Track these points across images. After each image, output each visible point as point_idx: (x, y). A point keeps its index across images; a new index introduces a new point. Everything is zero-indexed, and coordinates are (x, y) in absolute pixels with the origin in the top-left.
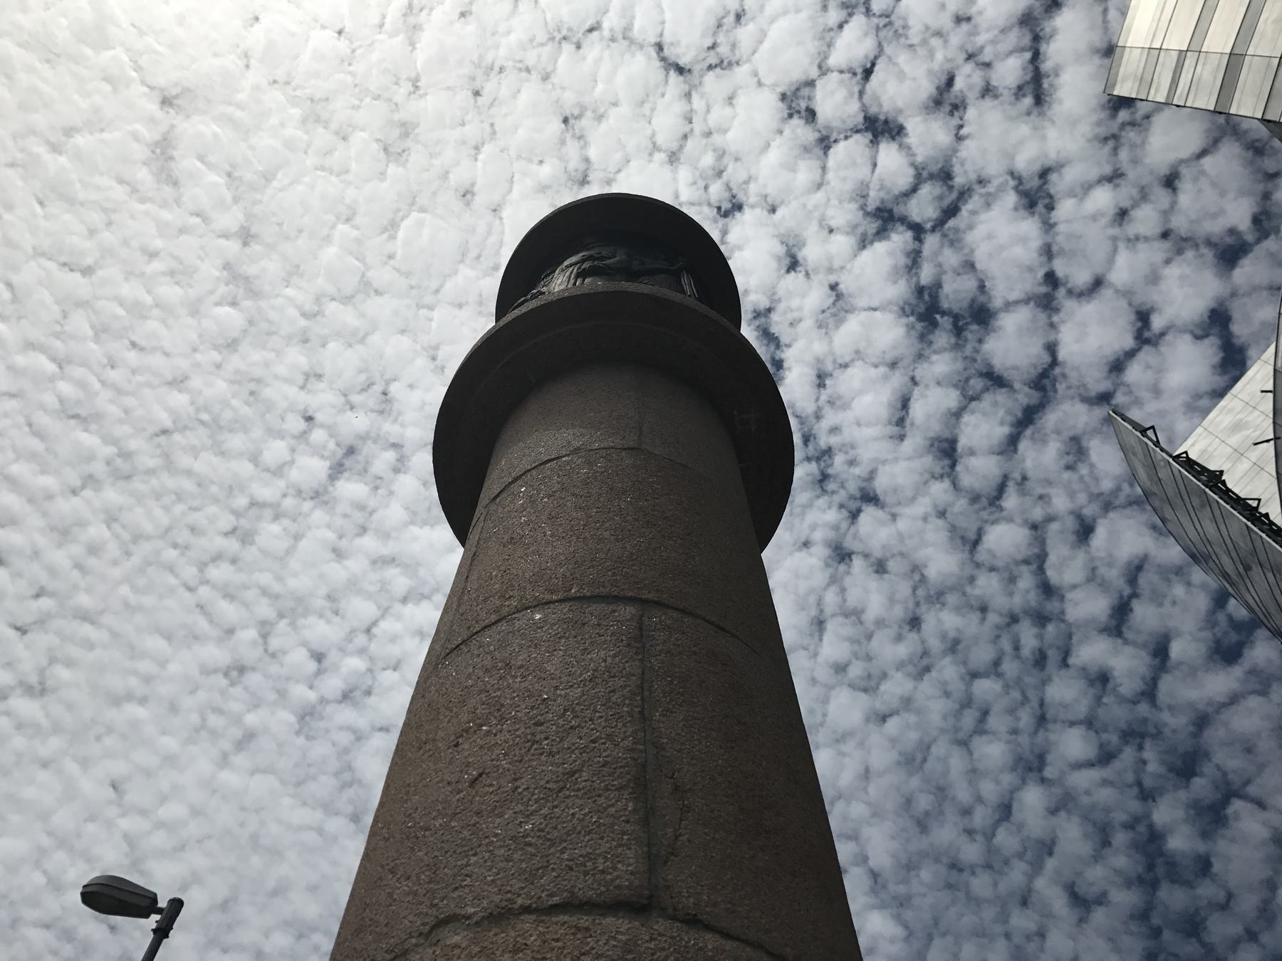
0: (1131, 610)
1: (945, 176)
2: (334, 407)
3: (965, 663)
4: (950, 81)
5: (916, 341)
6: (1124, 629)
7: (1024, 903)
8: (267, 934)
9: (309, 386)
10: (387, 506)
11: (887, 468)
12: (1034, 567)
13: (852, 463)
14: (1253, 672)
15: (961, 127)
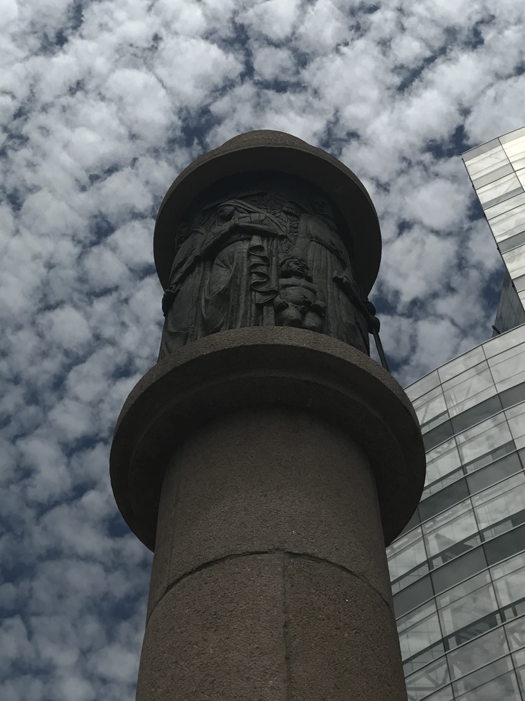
0: (93, 448)
1: (302, 60)
4: (373, 9)
5: (165, 139)
6: (74, 455)
11: (49, 196)
12: (66, 361)
13: (31, 165)
14: (117, 553)
15: (346, 44)
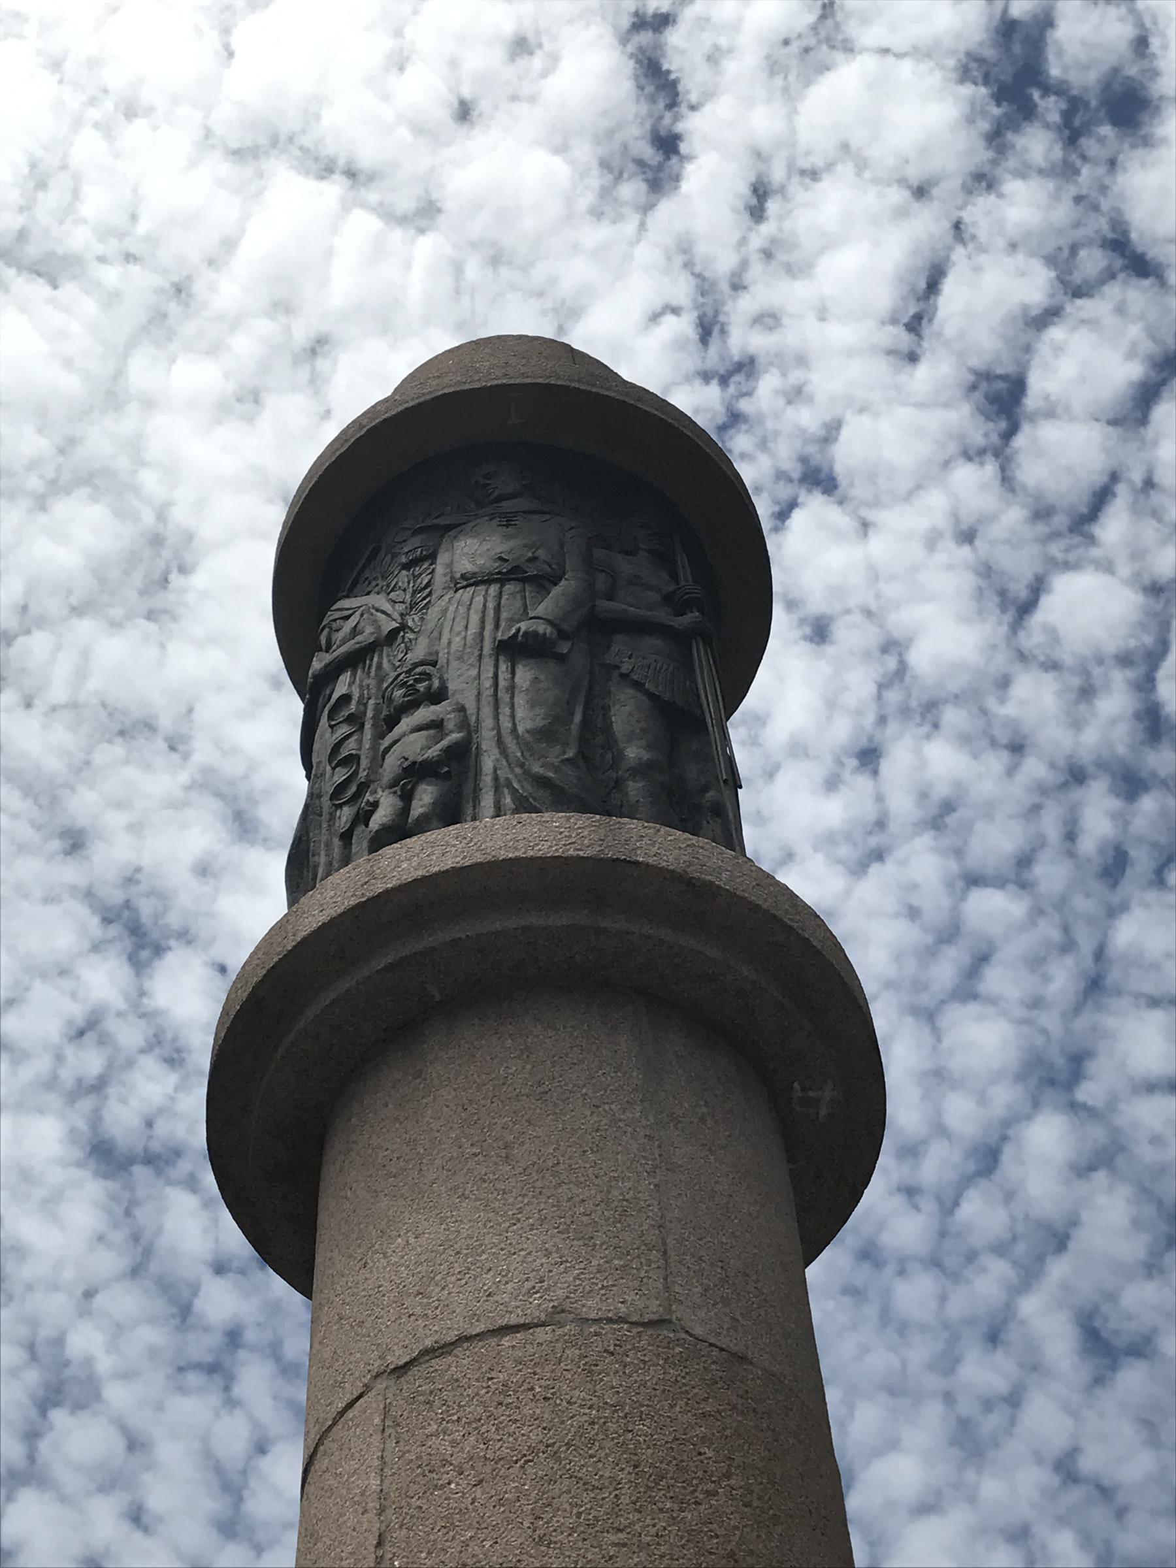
3: (958, 853)
5: (980, 144)
7: (993, 1338)
13: (796, 395)
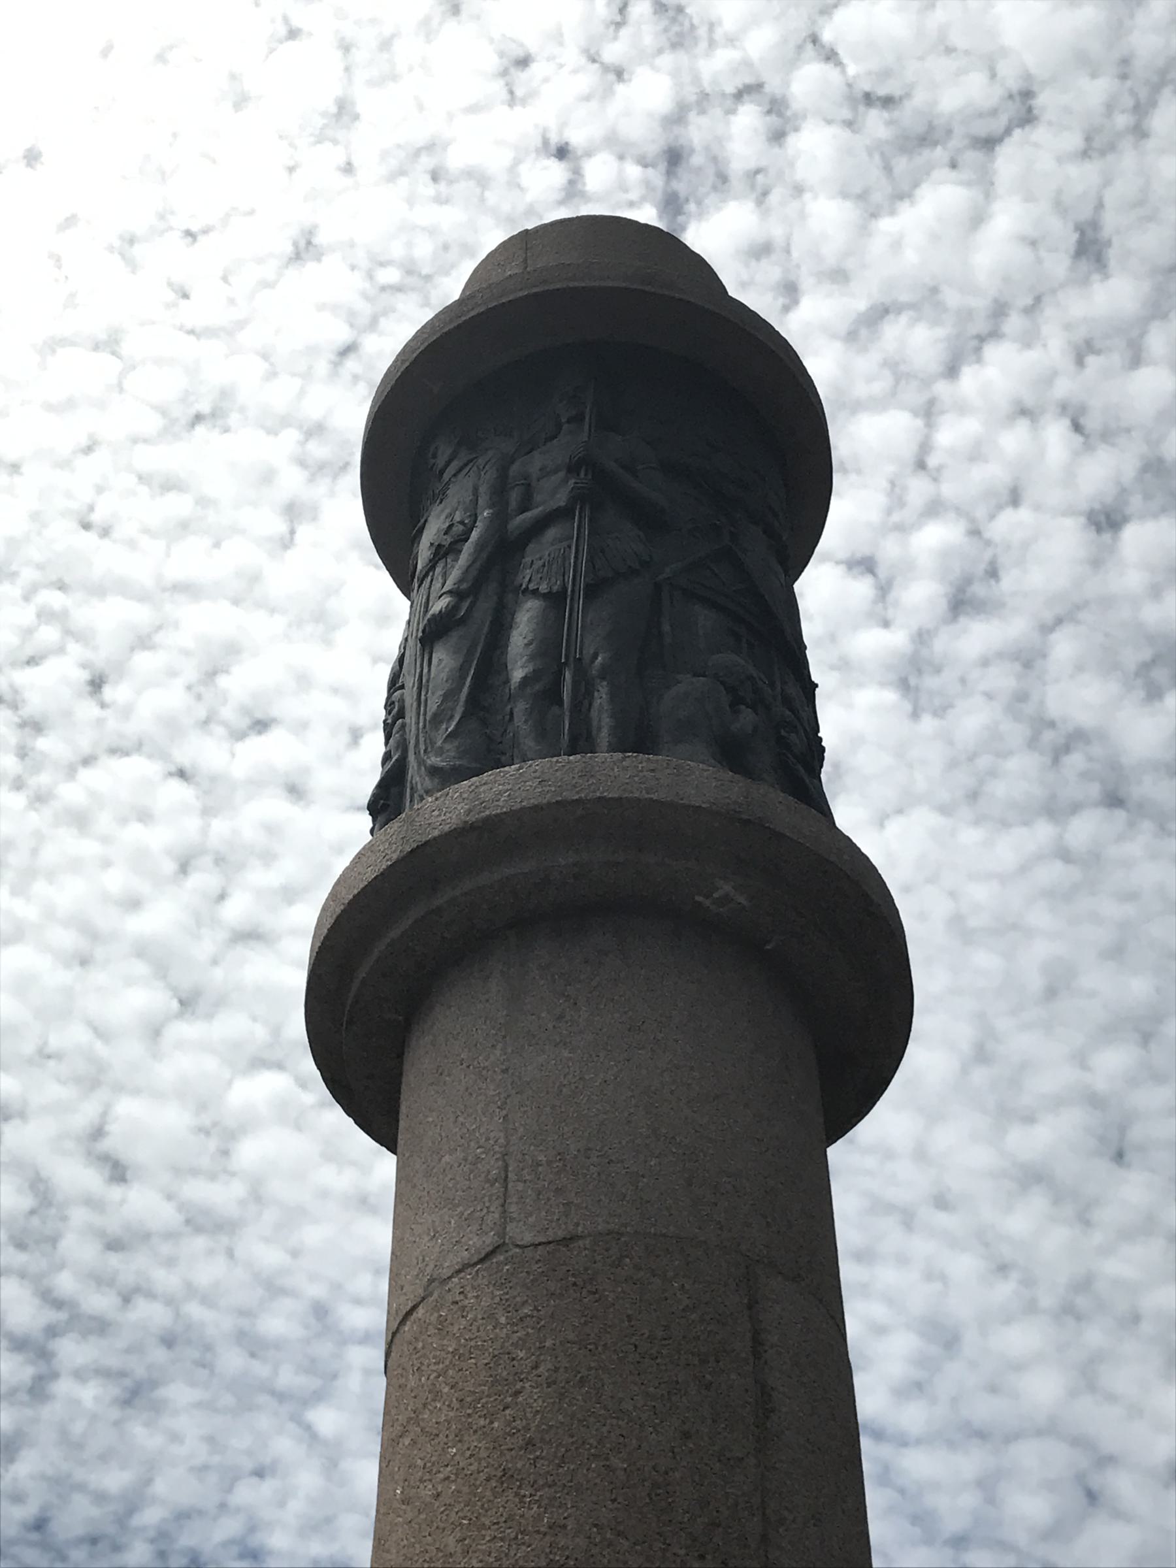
2: (587, 98)
8: (1081, 1060)
9: (519, 93)
10: (803, 215)
